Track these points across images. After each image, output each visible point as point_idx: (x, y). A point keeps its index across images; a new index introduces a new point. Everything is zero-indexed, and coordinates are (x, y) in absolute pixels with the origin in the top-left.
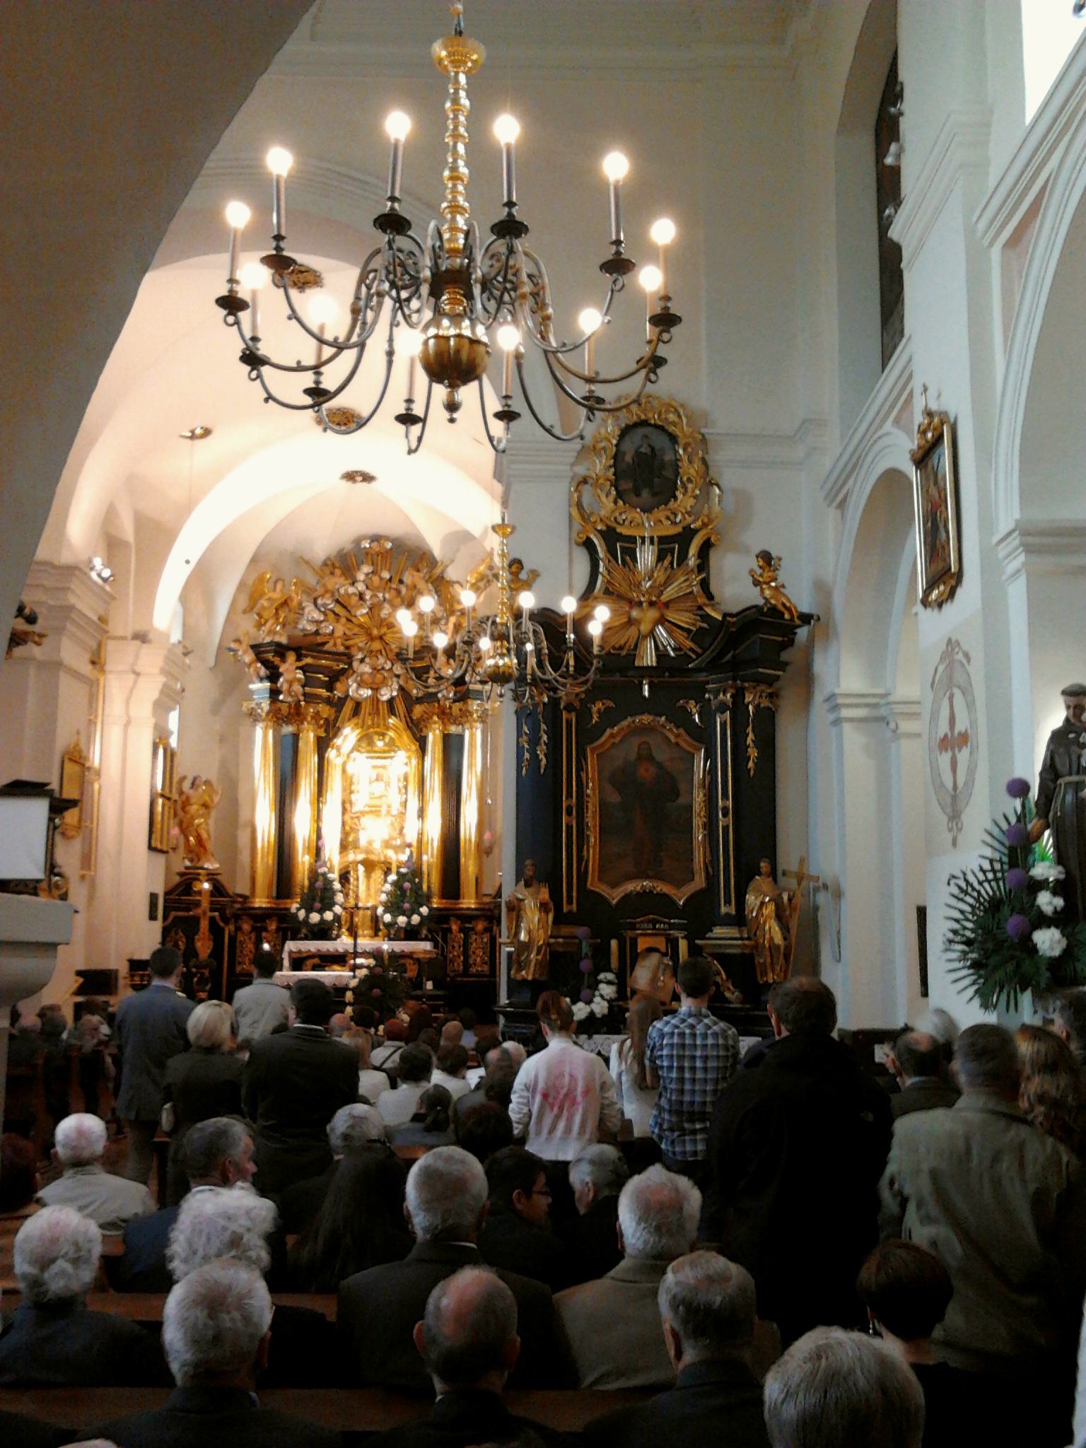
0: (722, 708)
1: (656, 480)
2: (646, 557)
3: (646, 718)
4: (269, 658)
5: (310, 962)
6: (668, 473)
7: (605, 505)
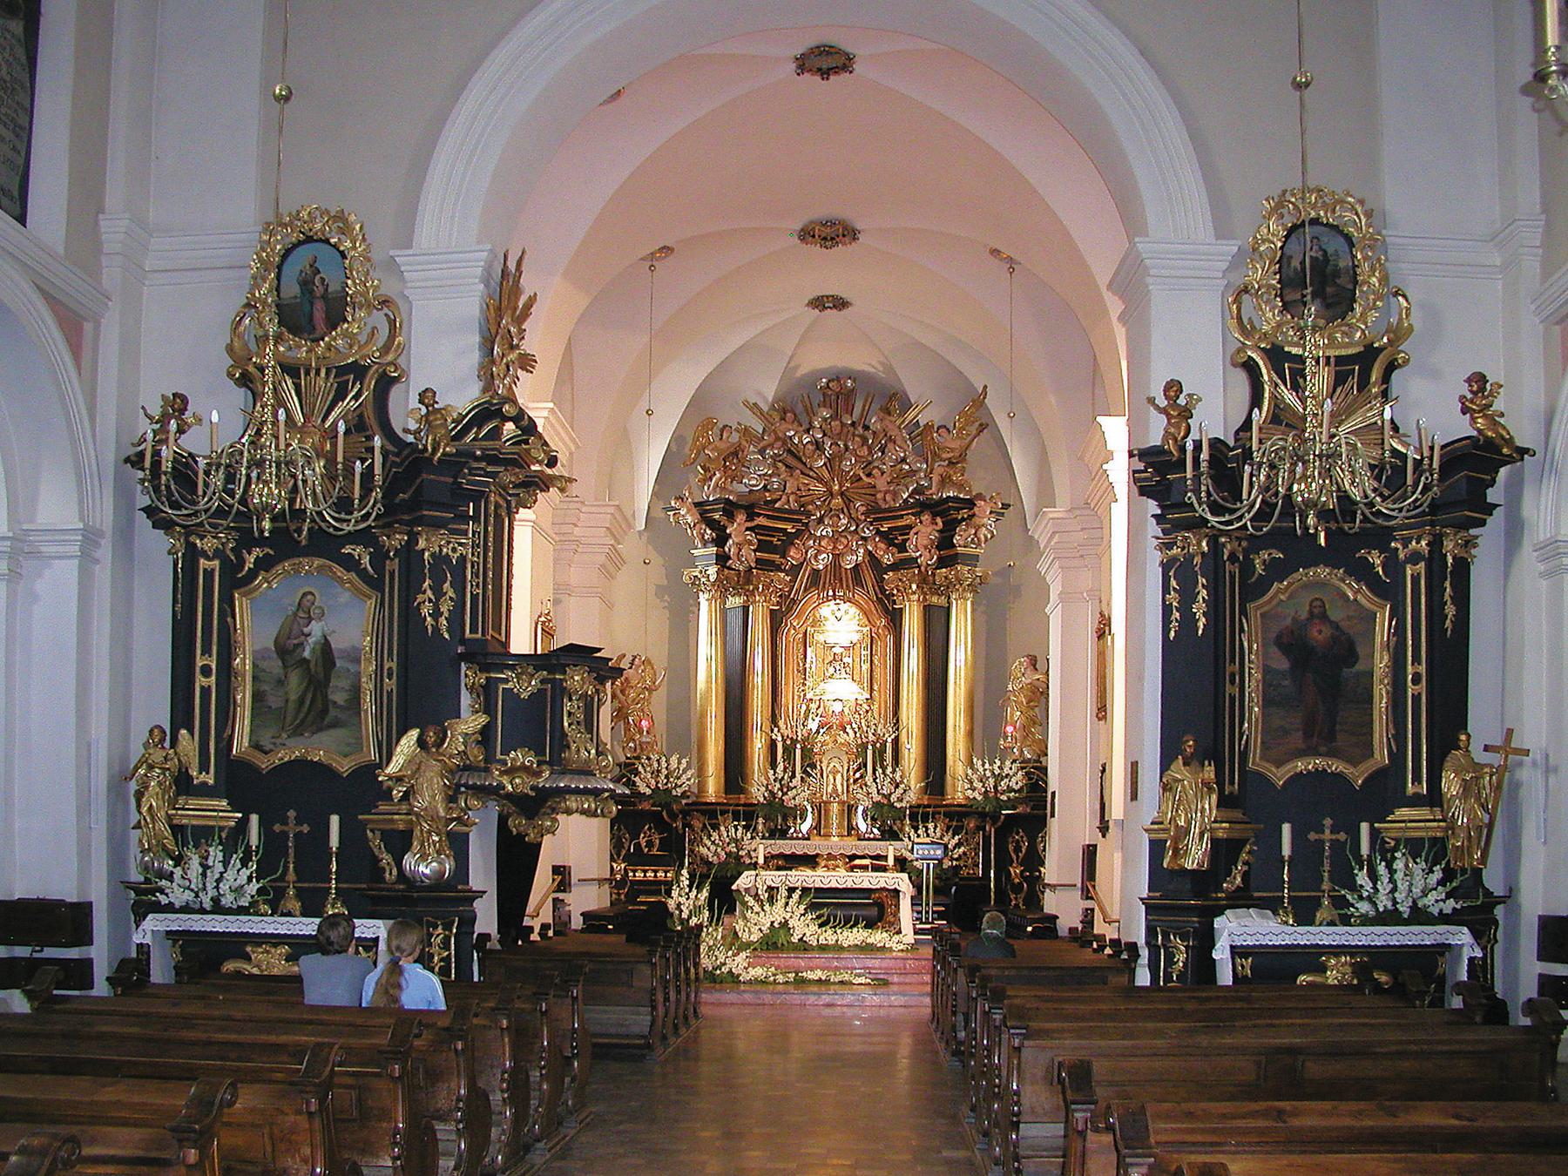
0: (1415, 558)
1: (1329, 290)
2: (1319, 380)
3: (1323, 572)
4: (714, 520)
6: (1343, 281)
7: (1269, 317)
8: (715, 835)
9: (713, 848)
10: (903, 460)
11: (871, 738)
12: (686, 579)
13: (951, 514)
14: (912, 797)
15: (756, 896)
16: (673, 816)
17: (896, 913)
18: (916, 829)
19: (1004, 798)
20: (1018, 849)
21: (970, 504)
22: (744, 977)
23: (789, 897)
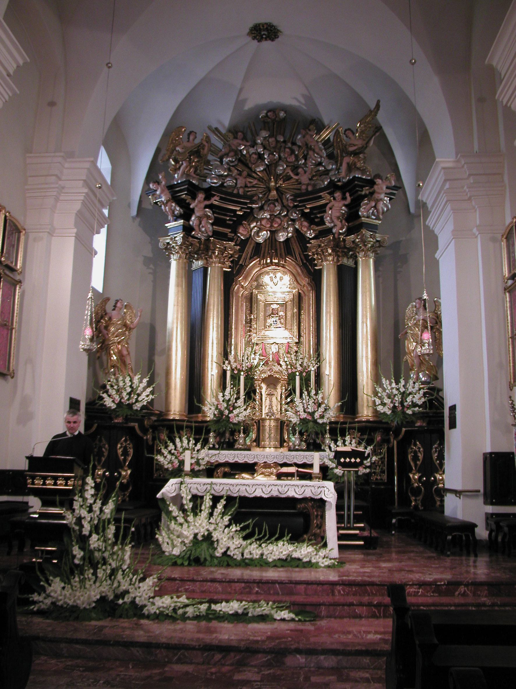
4: (183, 197)
5: (220, 470)
8: (171, 447)
9: (169, 457)
10: (320, 164)
11: (299, 368)
12: (161, 245)
13: (356, 192)
14: (332, 415)
15: (182, 509)
16: (145, 431)
17: (322, 526)
18: (336, 441)
19: (409, 412)
20: (415, 458)
21: (371, 183)
22: (152, 609)
23: (214, 507)
